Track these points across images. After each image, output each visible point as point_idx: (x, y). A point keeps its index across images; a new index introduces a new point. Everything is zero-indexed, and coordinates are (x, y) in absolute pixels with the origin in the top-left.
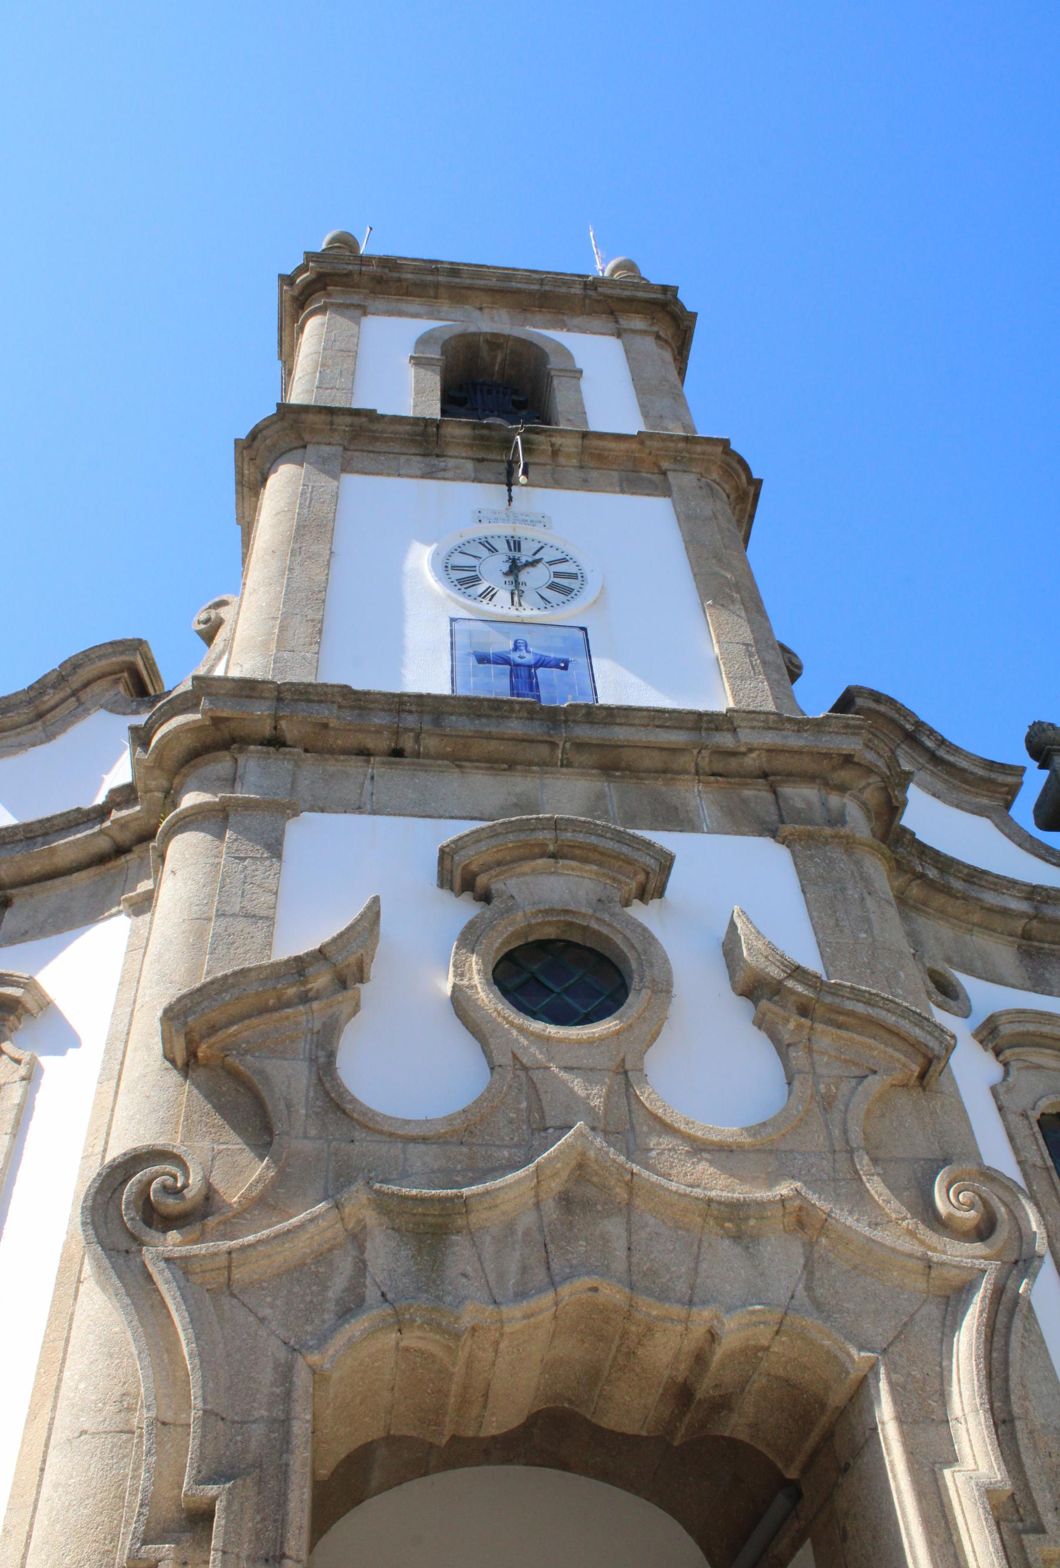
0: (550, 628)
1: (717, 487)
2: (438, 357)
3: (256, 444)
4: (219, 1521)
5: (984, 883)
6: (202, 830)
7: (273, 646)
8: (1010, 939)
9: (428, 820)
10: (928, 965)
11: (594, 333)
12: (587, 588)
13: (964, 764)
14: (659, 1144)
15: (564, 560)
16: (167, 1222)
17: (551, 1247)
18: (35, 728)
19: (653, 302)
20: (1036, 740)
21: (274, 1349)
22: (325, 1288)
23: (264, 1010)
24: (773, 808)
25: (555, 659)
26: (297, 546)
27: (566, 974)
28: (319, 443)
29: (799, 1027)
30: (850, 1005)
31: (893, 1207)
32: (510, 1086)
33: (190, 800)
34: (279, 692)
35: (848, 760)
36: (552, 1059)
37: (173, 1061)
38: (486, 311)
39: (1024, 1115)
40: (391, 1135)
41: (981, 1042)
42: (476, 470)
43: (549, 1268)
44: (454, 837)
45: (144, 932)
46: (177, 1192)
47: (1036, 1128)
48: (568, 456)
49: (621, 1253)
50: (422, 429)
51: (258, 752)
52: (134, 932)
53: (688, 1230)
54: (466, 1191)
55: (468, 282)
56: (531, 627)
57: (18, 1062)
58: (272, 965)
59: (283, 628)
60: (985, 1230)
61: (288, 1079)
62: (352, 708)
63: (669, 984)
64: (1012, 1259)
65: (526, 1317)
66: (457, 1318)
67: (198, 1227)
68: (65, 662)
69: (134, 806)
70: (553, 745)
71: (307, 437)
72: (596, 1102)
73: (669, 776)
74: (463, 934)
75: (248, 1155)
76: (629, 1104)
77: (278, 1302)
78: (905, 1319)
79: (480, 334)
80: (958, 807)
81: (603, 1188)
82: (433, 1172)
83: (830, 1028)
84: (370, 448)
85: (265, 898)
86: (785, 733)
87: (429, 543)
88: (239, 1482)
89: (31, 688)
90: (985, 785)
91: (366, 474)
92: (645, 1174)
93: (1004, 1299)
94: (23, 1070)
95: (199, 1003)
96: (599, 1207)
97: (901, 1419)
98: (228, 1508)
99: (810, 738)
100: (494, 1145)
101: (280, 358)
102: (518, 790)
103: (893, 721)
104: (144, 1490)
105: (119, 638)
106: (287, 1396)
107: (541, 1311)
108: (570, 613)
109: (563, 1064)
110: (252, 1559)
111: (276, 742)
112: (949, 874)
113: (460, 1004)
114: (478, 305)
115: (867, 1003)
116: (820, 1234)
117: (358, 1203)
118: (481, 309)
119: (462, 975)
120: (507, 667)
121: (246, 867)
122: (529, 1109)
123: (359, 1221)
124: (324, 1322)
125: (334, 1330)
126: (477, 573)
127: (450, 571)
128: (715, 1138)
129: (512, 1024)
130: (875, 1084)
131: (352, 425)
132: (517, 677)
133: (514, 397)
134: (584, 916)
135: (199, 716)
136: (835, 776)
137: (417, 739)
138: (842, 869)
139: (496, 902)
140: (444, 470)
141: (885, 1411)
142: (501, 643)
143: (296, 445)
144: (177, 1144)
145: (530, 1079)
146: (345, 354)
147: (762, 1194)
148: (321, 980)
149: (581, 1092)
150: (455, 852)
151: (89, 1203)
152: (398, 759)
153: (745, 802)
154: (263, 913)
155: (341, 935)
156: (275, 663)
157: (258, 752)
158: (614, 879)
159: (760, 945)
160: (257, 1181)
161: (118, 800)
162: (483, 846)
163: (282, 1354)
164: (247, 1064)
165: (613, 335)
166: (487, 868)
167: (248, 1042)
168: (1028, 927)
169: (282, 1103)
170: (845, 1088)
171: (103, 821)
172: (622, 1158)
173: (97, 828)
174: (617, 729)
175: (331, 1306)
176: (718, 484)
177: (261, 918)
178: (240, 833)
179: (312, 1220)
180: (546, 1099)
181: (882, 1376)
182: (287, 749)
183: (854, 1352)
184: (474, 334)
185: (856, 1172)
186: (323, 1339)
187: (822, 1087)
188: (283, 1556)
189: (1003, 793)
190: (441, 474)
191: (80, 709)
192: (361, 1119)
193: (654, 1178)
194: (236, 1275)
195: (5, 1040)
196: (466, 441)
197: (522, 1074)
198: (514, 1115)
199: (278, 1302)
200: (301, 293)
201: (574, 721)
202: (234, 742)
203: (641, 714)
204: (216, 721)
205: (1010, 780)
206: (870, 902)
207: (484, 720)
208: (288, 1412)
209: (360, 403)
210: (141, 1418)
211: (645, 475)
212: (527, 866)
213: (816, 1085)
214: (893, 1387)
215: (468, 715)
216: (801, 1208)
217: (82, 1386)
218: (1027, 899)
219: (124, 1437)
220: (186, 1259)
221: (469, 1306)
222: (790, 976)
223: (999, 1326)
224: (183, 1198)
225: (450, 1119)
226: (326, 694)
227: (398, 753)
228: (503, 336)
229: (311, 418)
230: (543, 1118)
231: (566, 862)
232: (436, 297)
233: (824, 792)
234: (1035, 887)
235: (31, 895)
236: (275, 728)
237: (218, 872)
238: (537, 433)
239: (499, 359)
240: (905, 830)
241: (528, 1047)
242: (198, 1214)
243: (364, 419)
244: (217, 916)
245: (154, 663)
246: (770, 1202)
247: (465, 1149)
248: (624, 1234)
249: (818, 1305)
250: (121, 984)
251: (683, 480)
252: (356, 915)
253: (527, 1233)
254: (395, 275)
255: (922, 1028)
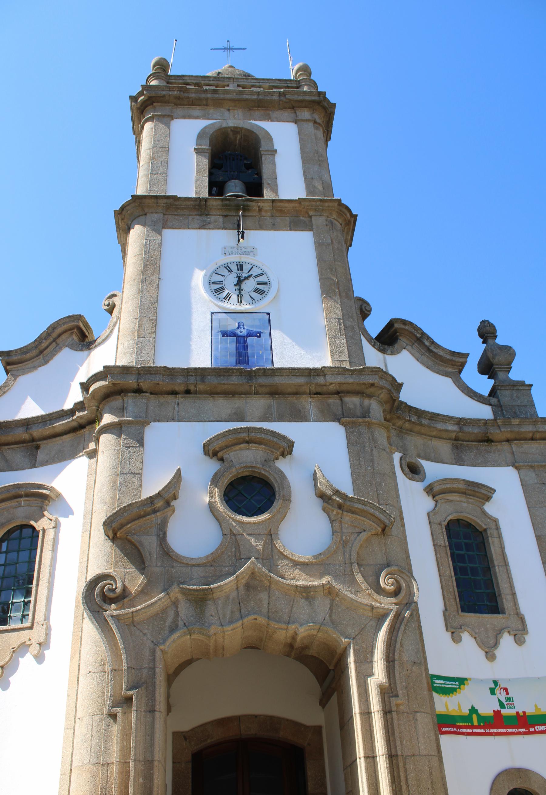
0: (254, 314)
1: (335, 222)
2: (207, 148)
3: (124, 212)
4: (134, 701)
5: (438, 419)
6: (112, 434)
7: (136, 334)
8: (449, 441)
9: (201, 423)
10: (408, 461)
11: (284, 122)
12: (271, 290)
13: (441, 353)
14: (282, 563)
15: (262, 274)
16: (112, 601)
17: (242, 604)
18: (39, 358)
19: (313, 102)
20: (481, 331)
21: (149, 644)
22: (165, 622)
23: (140, 517)
24: (340, 408)
25: (255, 332)
26: (144, 277)
27: (251, 491)
28: (152, 213)
29: (338, 513)
30: (356, 505)
31: (364, 585)
32: (229, 542)
33: (108, 419)
34: (139, 371)
35: (372, 385)
36: (244, 531)
37: (108, 537)
38: (231, 111)
39: (440, 524)
40: (186, 564)
41: (427, 493)
42: (224, 223)
43: (240, 612)
44: (209, 439)
45: (94, 467)
46: (113, 591)
47: (444, 530)
48: (266, 211)
49: (266, 605)
50: (198, 202)
51: (132, 396)
52: (90, 466)
53: (290, 596)
54: (212, 586)
55: (222, 96)
56: (246, 314)
57: (51, 520)
58: (141, 501)
59: (140, 325)
60: (396, 593)
61: (150, 543)
62: (168, 375)
63: (290, 497)
64: (406, 602)
65: (232, 630)
66: (209, 632)
67: (121, 602)
68: (49, 327)
69: (85, 411)
70: (251, 386)
71: (146, 210)
72: (260, 548)
73: (298, 396)
74: (212, 479)
75: (137, 573)
76: (272, 547)
77: (150, 628)
78: (363, 626)
79: (228, 127)
80: (438, 373)
81: (261, 581)
82: (201, 577)
83: (349, 514)
84: (176, 213)
85: (138, 465)
86: (346, 376)
87: (202, 270)
88: (140, 689)
89: (36, 340)
90: (451, 363)
91: (174, 228)
92: (275, 577)
93: (400, 618)
94: (53, 524)
95: (116, 518)
96: (259, 588)
97: (355, 662)
98: (137, 698)
99: (357, 378)
100: (223, 566)
101: (134, 134)
102: (236, 406)
103: (411, 332)
104: (111, 692)
105: (71, 314)
106: (154, 660)
107: (237, 628)
108: (263, 305)
109: (248, 533)
110: (145, 711)
111: (138, 391)
112: (422, 417)
113: (211, 507)
114: (227, 108)
115: (363, 504)
116: (336, 597)
117: (175, 592)
118: (229, 110)
119: (212, 497)
120: (235, 338)
121: (130, 451)
122: (236, 551)
123: (176, 598)
124: (165, 634)
125: (168, 637)
126: (223, 285)
127: (212, 285)
128: (302, 560)
129: (230, 517)
130: (364, 536)
131: (166, 203)
132: (239, 343)
133: (245, 162)
134: (259, 468)
135: (107, 383)
136: (368, 390)
137: (195, 386)
138: (365, 437)
139: (226, 463)
140: (209, 223)
141: (351, 659)
142: (232, 325)
143: (141, 214)
144: (110, 571)
145: (236, 539)
146: (163, 150)
147: (316, 583)
148: (159, 504)
149: (255, 544)
150: (209, 445)
151: (84, 595)
152: (188, 395)
153: (329, 405)
154: (138, 472)
155: (166, 486)
156: (137, 344)
157: (132, 396)
158: (271, 451)
159: (324, 481)
160: (141, 585)
161: (78, 407)
162: (220, 442)
163: (152, 646)
164: (134, 539)
165: (293, 122)
166: (222, 449)
167: (134, 530)
168: (458, 435)
169: (148, 554)
170: (353, 537)
171: (73, 416)
172: (267, 571)
173: (71, 419)
174: (276, 378)
175: (167, 628)
176: (336, 220)
177: (137, 474)
178: (127, 435)
179: (159, 600)
180: (242, 547)
181: (352, 647)
182: (144, 394)
183: (343, 639)
184: (225, 128)
185: (353, 572)
186: (165, 640)
187: (344, 537)
188: (155, 711)
189: (458, 366)
190: (208, 226)
191: (58, 348)
192: (176, 558)
193: (278, 578)
194: (135, 619)
195: (45, 511)
196: (219, 207)
197: (233, 537)
198: (232, 552)
199: (150, 628)
200: (141, 106)
201: (259, 375)
202: (123, 392)
203: (286, 371)
204: (114, 384)
205: (462, 360)
206: (375, 452)
207: (222, 377)
208: (154, 665)
209: (170, 193)
210: (108, 668)
211: (302, 218)
212: (237, 447)
213: (342, 536)
214: (354, 650)
215: (215, 376)
216: (330, 588)
217: (88, 656)
218: (457, 424)
219: (103, 673)
220: (118, 615)
221: (213, 627)
222: (334, 494)
223: (396, 628)
224: (116, 593)
225: (207, 557)
226: (158, 371)
227: (188, 392)
228: (240, 128)
229: (147, 201)
230: (240, 554)
231: (253, 445)
232: (207, 105)
233: (362, 399)
234: (461, 419)
235: (47, 444)
236: (138, 385)
237: (119, 453)
238: (251, 201)
239: (238, 138)
240: (402, 403)
241: (236, 526)
242: (121, 597)
243: (172, 200)
244: (121, 474)
245: (87, 323)
246: (318, 586)
247: (212, 568)
248: (267, 598)
249: (332, 622)
250: (87, 489)
251: (319, 221)
252: (173, 475)
253: (233, 599)
254: (186, 95)
255: (383, 514)
